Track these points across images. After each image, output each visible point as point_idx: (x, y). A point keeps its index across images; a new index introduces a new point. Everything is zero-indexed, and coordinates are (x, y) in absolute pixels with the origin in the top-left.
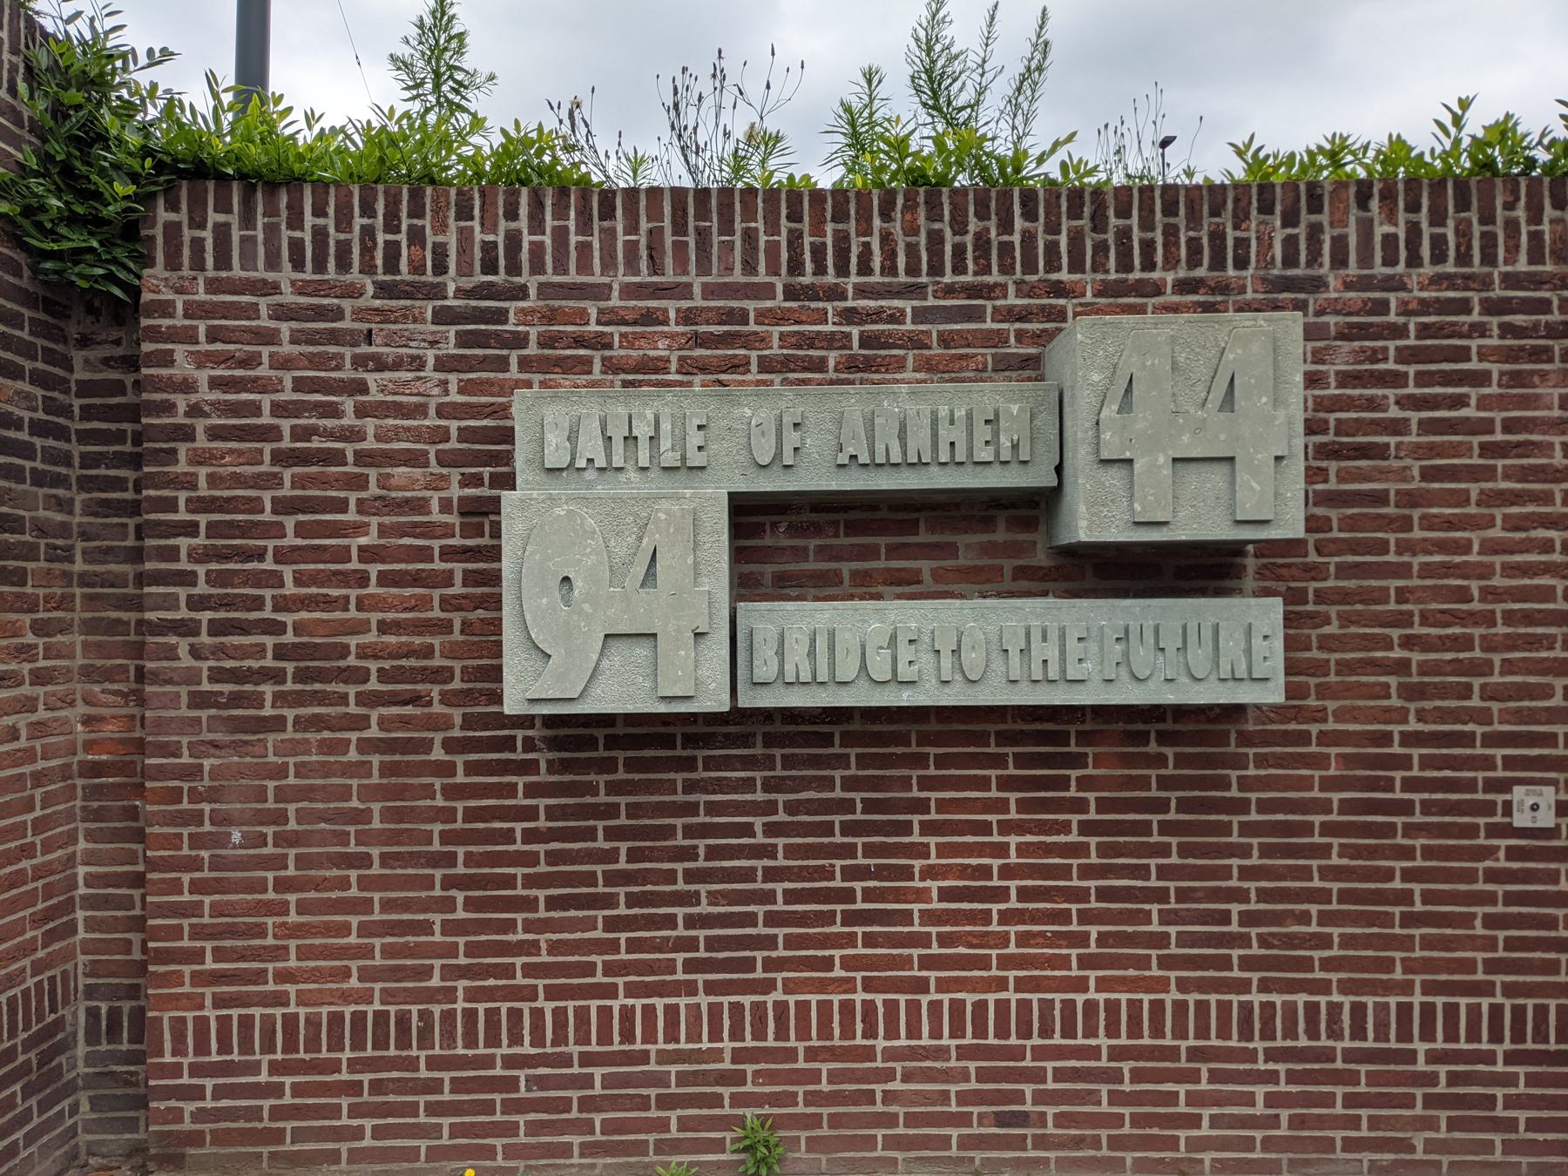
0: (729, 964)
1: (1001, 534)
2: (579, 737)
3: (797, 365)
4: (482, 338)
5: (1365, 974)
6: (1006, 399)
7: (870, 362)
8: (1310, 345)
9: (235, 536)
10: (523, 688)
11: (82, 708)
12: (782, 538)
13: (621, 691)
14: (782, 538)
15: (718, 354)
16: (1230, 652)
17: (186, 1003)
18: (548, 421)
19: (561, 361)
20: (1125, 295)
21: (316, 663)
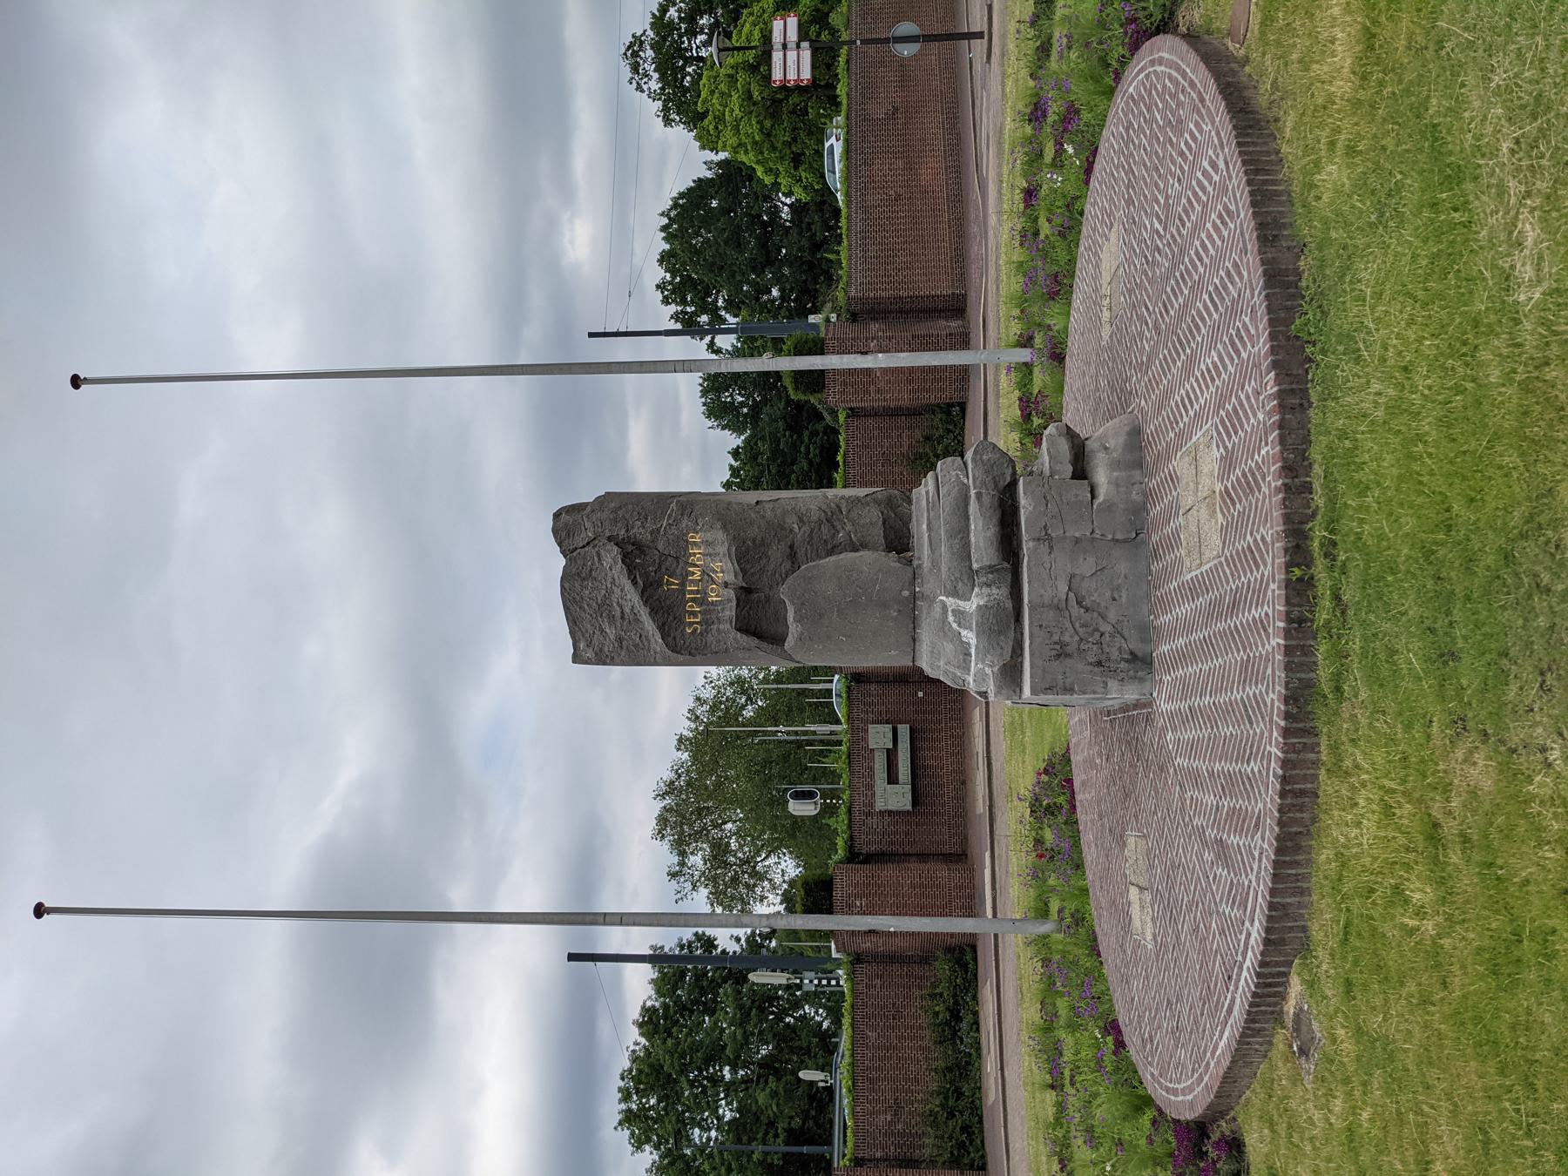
0: (941, 786)
1: (891, 755)
2: (915, 802)
3: (872, 777)
4: (868, 814)
5: (940, 713)
6: (877, 754)
7: (871, 769)
8: (837, 683)
9: (892, 843)
10: (909, 807)
11: (1391, 148)
12: (892, 779)
13: (909, 796)
14: (892, 779)
15: (871, 787)
16: (904, 730)
17: (947, 849)
18: (880, 805)
19: (872, 805)
20: (865, 740)
21: (907, 834)
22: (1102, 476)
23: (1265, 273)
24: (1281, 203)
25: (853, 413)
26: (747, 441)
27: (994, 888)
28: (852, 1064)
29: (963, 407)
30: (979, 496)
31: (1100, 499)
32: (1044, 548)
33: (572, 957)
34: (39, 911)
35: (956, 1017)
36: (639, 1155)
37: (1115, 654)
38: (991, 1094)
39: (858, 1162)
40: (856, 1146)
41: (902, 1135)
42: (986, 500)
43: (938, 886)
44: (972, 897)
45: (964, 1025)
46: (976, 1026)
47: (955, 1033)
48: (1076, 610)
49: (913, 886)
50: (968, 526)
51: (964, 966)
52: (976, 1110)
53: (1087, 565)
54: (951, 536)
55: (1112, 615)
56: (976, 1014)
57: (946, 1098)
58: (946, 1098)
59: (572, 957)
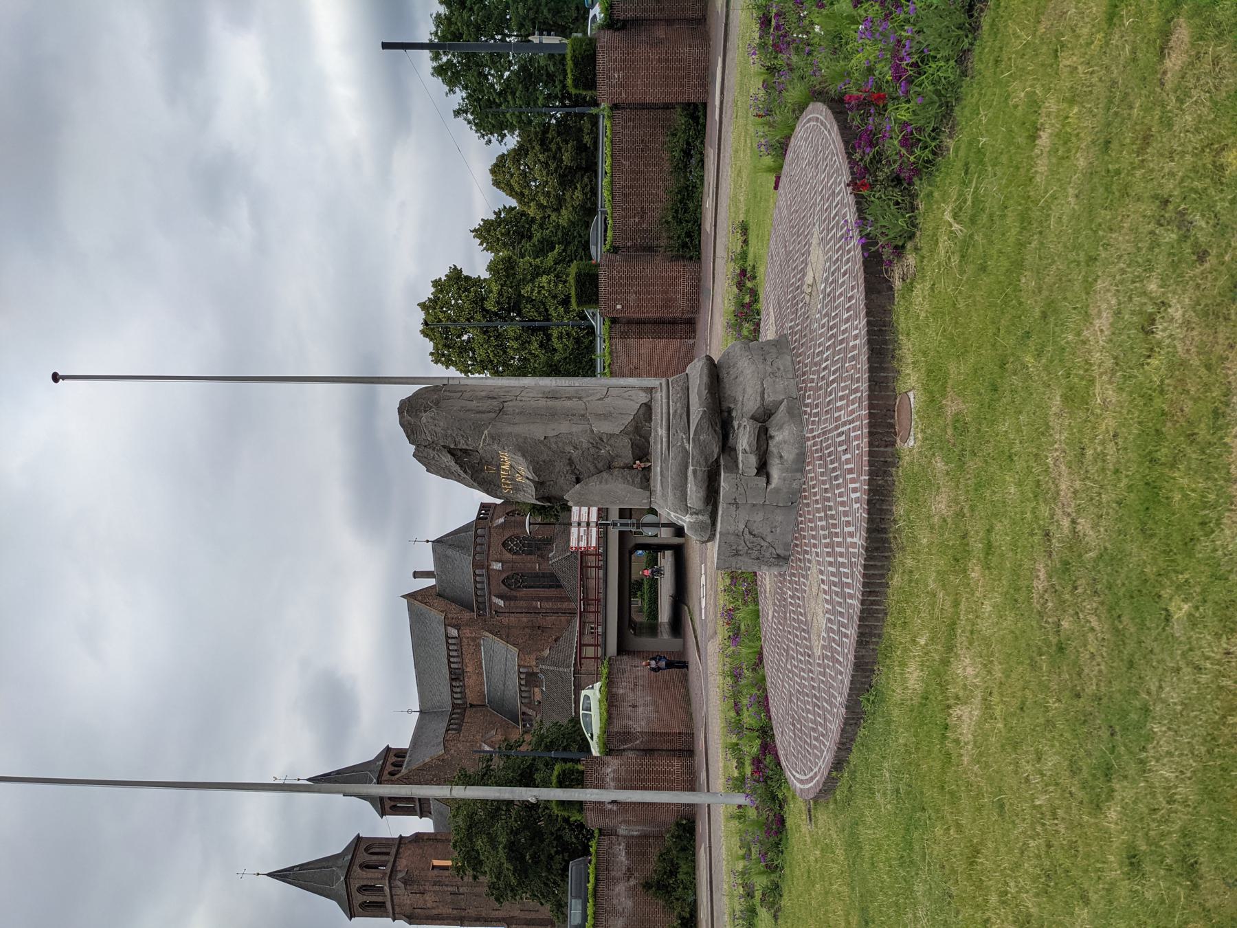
9: (645, 10)
17: (690, 14)
22: (775, 473)
23: (855, 664)
24: (877, 619)
25: (615, 107)
26: (519, 135)
27: (722, 93)
28: (612, 182)
29: (705, 105)
30: (694, 472)
31: (773, 486)
32: (733, 508)
33: (386, 46)
34: (56, 378)
35: (687, 154)
36: (451, 96)
37: (768, 555)
38: (708, 225)
39: (615, 250)
40: (614, 236)
41: (645, 231)
42: (699, 474)
43: (680, 61)
44: (706, 69)
45: (693, 161)
46: (702, 162)
47: (686, 167)
48: (747, 536)
49: (659, 61)
50: (686, 483)
51: (695, 119)
52: (698, 222)
53: (758, 517)
54: (675, 488)
55: (769, 539)
56: (702, 154)
57: (677, 212)
58: (677, 212)
59: (386, 46)
